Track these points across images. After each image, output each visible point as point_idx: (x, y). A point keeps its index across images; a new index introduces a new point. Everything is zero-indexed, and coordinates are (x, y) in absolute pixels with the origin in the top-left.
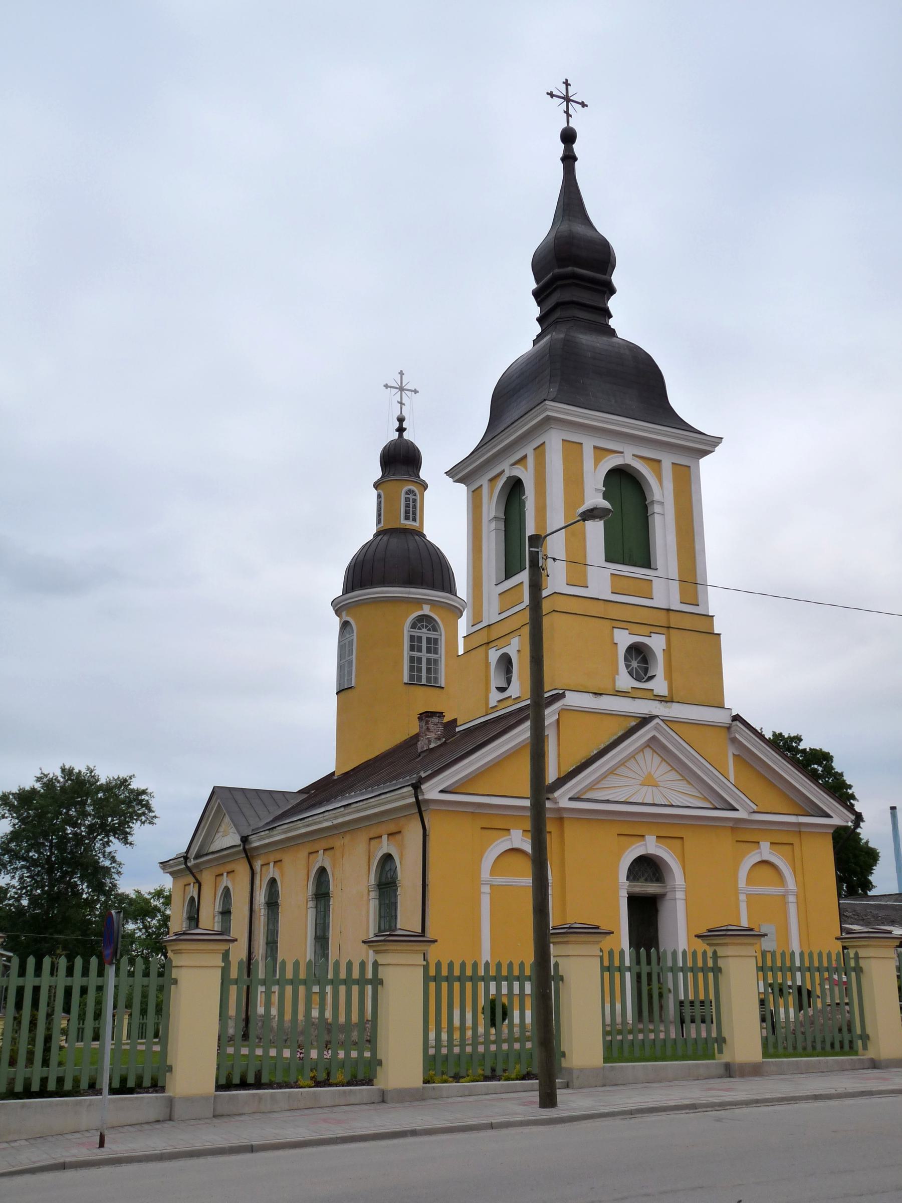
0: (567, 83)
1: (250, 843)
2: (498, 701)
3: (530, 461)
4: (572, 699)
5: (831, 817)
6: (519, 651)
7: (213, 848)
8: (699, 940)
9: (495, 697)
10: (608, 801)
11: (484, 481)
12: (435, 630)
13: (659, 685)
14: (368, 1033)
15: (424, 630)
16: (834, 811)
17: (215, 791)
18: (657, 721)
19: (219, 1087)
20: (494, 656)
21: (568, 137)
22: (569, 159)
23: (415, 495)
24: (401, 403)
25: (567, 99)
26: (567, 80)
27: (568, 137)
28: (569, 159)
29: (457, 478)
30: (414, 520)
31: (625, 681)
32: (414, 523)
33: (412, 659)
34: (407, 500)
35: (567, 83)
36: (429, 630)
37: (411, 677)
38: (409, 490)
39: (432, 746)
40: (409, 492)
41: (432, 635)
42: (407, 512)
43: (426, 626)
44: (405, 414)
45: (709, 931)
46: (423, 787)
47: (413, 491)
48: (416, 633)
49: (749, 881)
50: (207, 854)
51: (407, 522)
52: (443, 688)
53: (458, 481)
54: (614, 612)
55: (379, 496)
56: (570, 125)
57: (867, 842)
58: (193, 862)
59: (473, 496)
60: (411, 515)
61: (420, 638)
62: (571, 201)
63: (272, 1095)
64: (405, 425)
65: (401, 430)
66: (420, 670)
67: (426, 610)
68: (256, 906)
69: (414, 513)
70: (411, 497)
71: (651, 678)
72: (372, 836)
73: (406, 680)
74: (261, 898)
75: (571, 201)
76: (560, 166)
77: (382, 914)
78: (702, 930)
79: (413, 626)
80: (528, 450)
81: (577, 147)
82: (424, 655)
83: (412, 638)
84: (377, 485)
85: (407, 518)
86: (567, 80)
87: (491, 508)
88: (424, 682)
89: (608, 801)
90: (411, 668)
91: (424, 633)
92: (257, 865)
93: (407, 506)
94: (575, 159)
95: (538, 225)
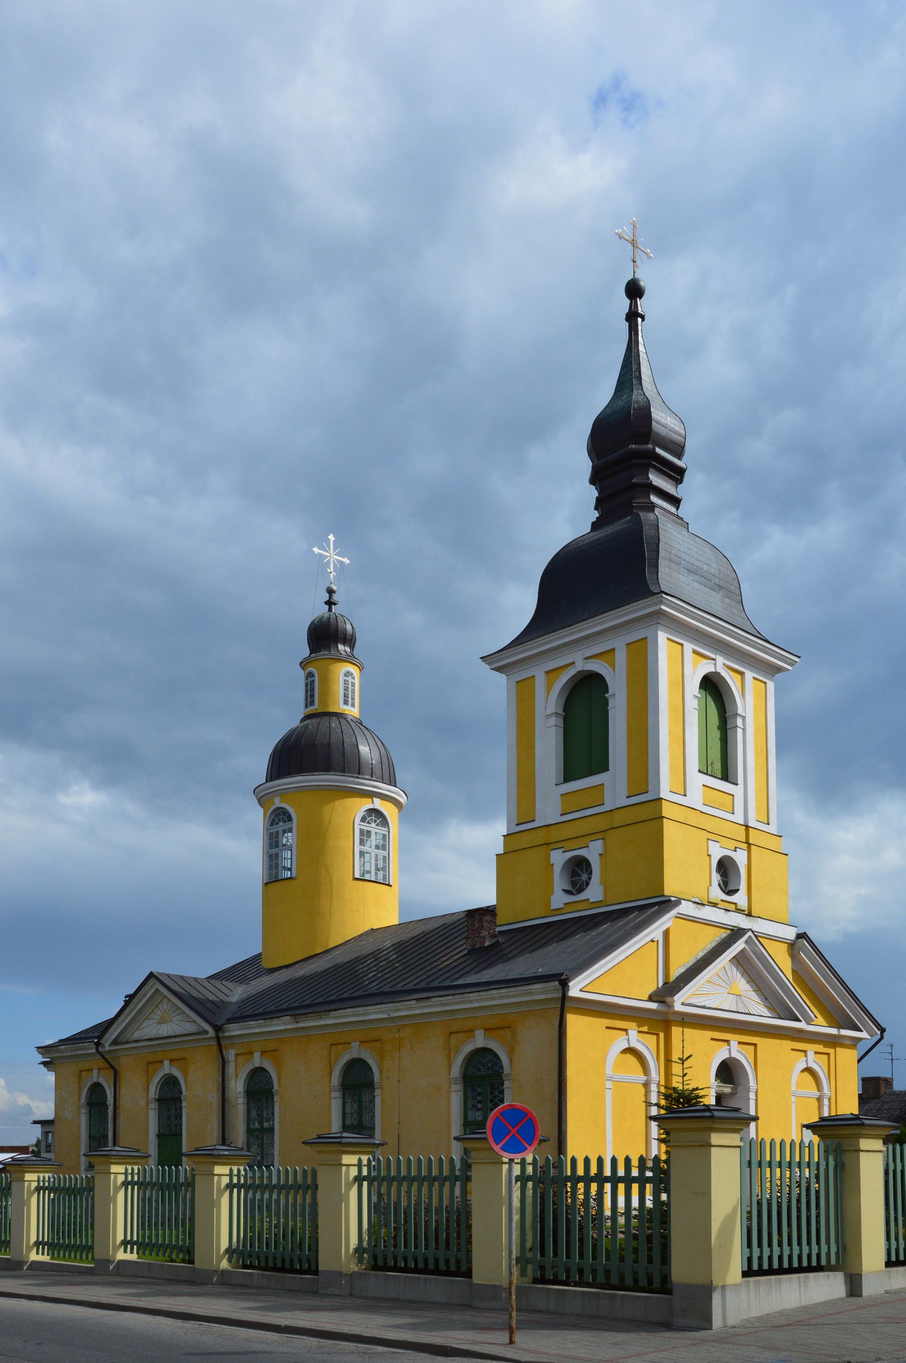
1: (223, 1032)
2: (565, 904)
3: (621, 657)
4: (686, 908)
5: (861, 1031)
6: (601, 855)
7: (137, 1035)
8: (308, 1147)
9: (559, 899)
10: (704, 1007)
11: (538, 672)
13: (741, 898)
14: (460, 1222)
16: (864, 1026)
17: (151, 975)
18: (750, 933)
19: (889, 1264)
20: (559, 858)
23: (353, 678)
29: (493, 666)
31: (717, 894)
32: (352, 709)
34: (346, 682)
36: (285, 822)
38: (348, 672)
39: (487, 944)
42: (346, 696)
43: (375, 821)
45: (319, 1137)
46: (570, 984)
47: (352, 674)
49: (797, 1085)
50: (127, 1042)
51: (345, 707)
53: (498, 669)
54: (707, 823)
55: (310, 675)
58: (107, 1048)
59: (517, 687)
60: (350, 699)
61: (369, 832)
63: (425, 1278)
64: (335, 597)
65: (330, 603)
67: (378, 804)
68: (230, 1094)
70: (349, 679)
71: (736, 891)
72: (454, 1030)
74: (237, 1086)
77: (470, 1106)
78: (311, 1136)
79: (363, 819)
80: (620, 643)
84: (303, 664)
85: (346, 702)
87: (548, 703)
89: (704, 1007)
92: (231, 1055)
93: (346, 689)
95: (601, 395)
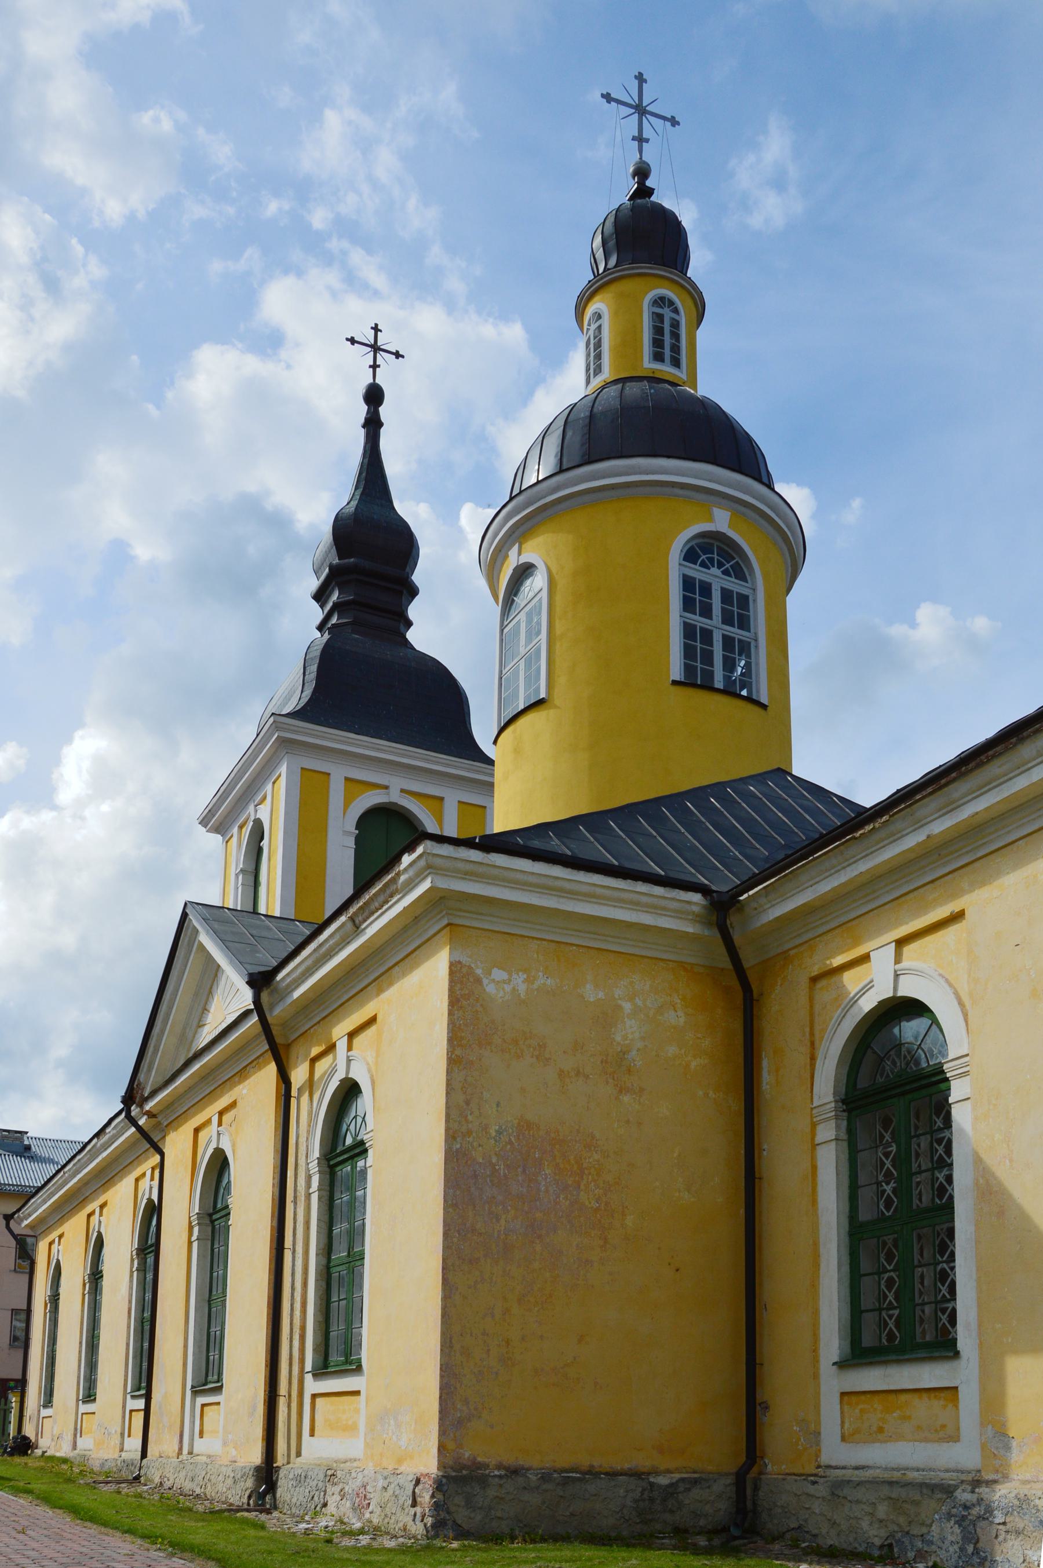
0: (376, 329)
12: (740, 575)
15: (715, 571)
21: (374, 396)
22: (373, 425)
24: (640, 139)
25: (375, 348)
26: (376, 325)
27: (374, 396)
28: (373, 425)
30: (676, 363)
33: (689, 631)
34: (659, 318)
35: (376, 329)
37: (689, 669)
40: (661, 301)
41: (734, 585)
43: (720, 565)
44: (650, 155)
47: (671, 303)
48: (697, 573)
51: (657, 366)
52: (764, 707)
56: (377, 381)
57: (929, 1399)
62: (372, 476)
66: (708, 658)
69: (676, 349)
73: (676, 672)
75: (372, 476)
76: (362, 433)
81: (385, 411)
82: (719, 629)
83: (688, 583)
85: (658, 357)
86: (376, 325)
88: (719, 683)
90: (689, 652)
91: (716, 579)
93: (658, 330)
94: (381, 425)
